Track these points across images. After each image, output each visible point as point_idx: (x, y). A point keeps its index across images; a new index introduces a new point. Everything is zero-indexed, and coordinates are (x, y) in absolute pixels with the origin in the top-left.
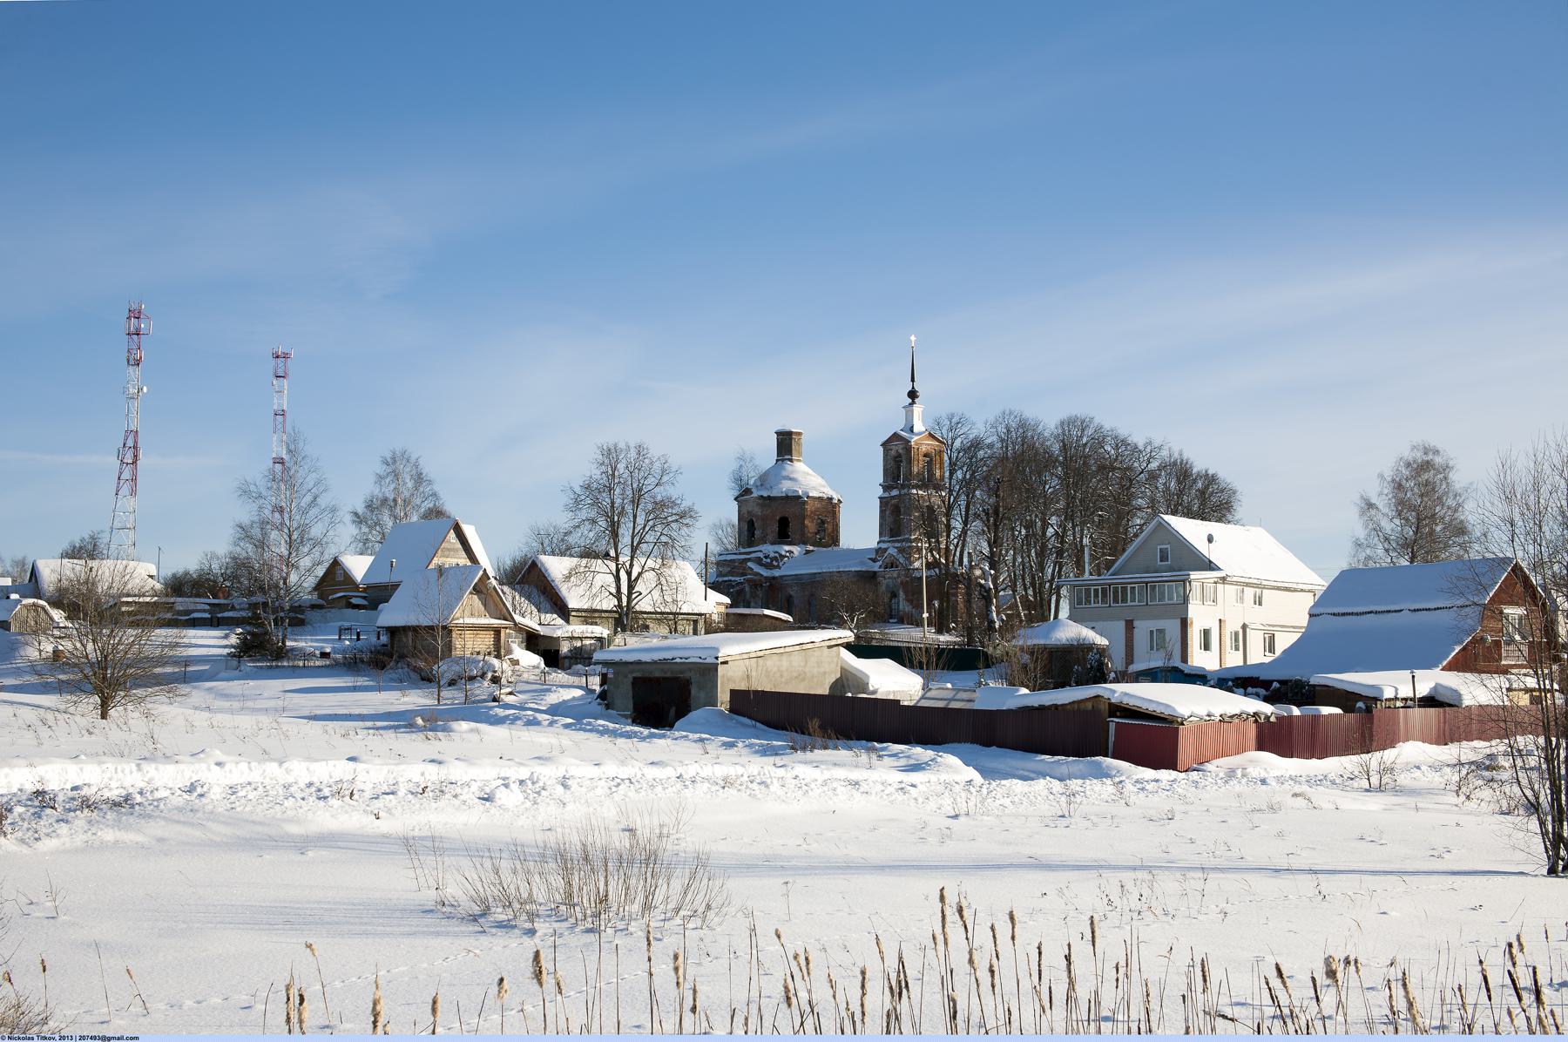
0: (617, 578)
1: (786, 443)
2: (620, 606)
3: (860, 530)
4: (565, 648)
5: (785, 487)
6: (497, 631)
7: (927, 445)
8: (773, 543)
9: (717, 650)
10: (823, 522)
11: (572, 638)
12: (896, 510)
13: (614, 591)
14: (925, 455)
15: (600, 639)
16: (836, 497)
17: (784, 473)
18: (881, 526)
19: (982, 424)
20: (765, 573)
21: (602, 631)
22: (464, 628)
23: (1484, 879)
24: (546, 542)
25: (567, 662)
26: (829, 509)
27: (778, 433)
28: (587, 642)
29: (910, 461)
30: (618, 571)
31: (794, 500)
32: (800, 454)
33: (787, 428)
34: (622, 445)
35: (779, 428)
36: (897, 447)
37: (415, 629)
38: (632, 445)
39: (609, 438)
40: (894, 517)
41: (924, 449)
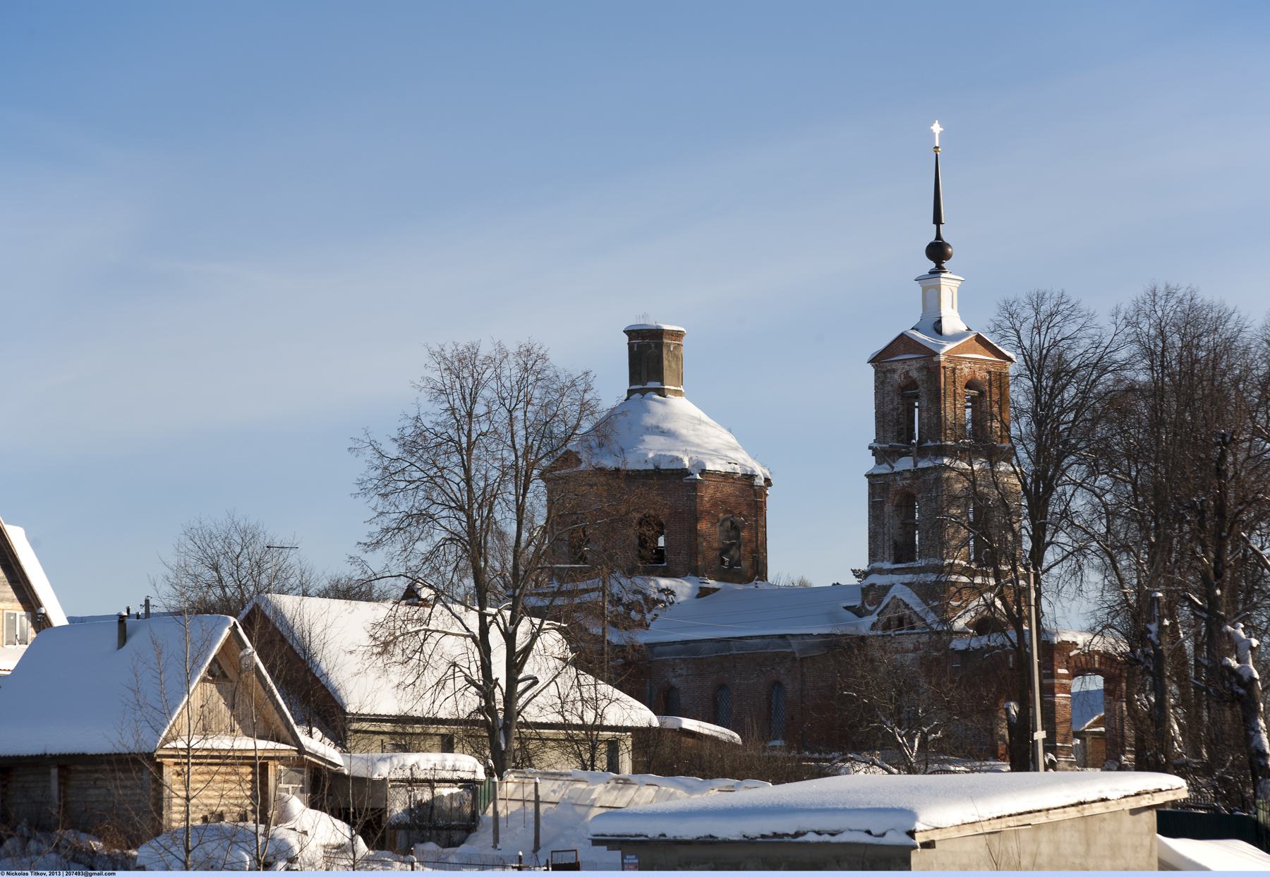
0: (485, 650)
1: (649, 355)
2: (489, 709)
3: (820, 543)
4: (398, 806)
5: (652, 450)
6: (260, 767)
7: (974, 363)
8: (631, 572)
9: (912, 815)
10: (735, 528)
11: (412, 782)
12: (906, 501)
13: (477, 675)
14: (969, 385)
15: (469, 784)
16: (760, 471)
17: (649, 421)
19: (1105, 315)
20: (614, 637)
21: (467, 764)
22: (188, 757)
24: (225, 565)
25: (401, 836)
26: (749, 496)
27: (632, 333)
28: (445, 791)
29: (936, 397)
30: (484, 629)
31: (675, 480)
32: (680, 380)
33: (653, 322)
34: (486, 350)
35: (634, 321)
37: (68, 764)
38: (512, 348)
39: (455, 339)
40: (901, 515)
41: (965, 370)
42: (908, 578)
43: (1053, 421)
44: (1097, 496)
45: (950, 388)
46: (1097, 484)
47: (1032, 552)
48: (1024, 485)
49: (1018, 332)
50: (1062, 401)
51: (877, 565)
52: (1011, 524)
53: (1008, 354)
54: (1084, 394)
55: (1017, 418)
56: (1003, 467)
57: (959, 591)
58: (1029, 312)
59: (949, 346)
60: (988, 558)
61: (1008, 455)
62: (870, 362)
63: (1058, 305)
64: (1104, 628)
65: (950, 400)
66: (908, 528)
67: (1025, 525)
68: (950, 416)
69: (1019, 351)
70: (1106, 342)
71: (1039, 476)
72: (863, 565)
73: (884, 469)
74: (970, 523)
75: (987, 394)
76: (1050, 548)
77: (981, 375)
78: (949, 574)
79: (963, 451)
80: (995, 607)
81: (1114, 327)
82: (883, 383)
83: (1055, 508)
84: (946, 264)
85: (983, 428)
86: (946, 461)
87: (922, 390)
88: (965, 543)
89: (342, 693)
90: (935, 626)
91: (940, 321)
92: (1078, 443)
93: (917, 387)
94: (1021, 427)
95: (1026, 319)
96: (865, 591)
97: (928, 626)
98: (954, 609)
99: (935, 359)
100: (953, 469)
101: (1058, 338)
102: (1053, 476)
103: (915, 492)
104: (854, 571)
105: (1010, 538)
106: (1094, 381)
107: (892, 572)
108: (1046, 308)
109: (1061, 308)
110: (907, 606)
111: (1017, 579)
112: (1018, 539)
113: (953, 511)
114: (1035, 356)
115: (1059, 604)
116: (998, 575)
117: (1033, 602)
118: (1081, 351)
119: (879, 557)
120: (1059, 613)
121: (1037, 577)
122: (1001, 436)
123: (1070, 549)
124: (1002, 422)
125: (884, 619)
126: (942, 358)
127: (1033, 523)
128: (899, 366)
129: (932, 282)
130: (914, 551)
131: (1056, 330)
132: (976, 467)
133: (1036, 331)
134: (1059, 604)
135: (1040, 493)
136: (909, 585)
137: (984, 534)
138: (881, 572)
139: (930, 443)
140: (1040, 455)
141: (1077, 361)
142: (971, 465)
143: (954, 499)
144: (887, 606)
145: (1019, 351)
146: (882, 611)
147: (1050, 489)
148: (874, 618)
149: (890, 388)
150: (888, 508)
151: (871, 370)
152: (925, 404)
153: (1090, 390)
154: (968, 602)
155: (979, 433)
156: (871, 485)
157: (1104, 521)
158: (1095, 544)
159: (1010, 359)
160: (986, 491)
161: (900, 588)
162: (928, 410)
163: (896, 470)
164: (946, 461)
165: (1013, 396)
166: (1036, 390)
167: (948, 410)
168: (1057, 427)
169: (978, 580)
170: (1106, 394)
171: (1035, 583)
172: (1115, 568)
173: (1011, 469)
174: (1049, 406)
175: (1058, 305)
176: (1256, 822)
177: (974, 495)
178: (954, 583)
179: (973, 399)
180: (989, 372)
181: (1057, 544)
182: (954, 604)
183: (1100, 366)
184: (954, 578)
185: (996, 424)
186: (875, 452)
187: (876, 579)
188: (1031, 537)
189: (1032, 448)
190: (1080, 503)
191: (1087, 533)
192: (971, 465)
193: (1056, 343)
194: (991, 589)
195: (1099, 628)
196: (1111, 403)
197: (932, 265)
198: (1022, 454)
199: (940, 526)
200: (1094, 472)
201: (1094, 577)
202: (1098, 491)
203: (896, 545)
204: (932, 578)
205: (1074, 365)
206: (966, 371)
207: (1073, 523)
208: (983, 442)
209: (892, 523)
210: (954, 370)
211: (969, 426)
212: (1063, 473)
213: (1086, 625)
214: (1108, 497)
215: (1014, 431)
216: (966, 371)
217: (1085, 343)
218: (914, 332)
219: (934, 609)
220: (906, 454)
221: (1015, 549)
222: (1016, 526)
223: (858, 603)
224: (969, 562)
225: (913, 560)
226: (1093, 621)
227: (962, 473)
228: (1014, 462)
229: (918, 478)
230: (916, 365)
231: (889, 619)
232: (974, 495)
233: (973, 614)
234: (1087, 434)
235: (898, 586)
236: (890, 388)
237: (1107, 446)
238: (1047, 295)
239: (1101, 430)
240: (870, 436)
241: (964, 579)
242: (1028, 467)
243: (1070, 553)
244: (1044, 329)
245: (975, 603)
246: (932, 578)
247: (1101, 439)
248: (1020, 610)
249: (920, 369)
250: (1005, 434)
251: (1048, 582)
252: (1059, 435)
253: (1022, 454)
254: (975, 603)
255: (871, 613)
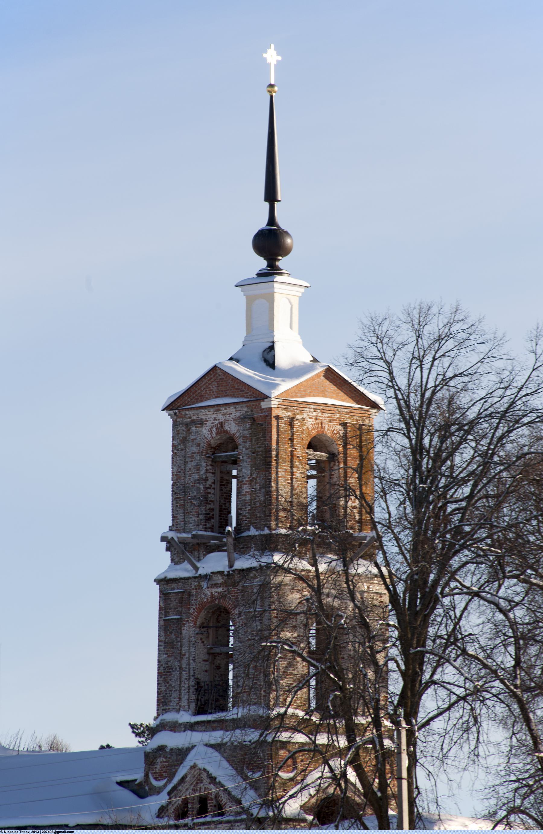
7: (321, 412)
12: (217, 619)
14: (314, 444)
18: (165, 673)
23: (289, 322)
29: (264, 461)
34: (205, 650)
36: (221, 416)
41: (309, 423)
42: (216, 736)
43: (439, 498)
44: (501, 611)
45: (285, 448)
46: (501, 593)
47: (403, 695)
48: (394, 597)
49: (389, 364)
50: (452, 467)
51: (170, 717)
52: (374, 653)
53: (373, 397)
54: (487, 459)
55: (384, 494)
56: (363, 567)
57: (293, 757)
58: (406, 334)
59: (285, 386)
60: (337, 703)
61: (370, 550)
62: (167, 408)
63: (450, 324)
64: (513, 811)
65: (284, 466)
66: (218, 659)
67: (393, 657)
68: (284, 489)
69: (391, 393)
70: (520, 380)
71: (416, 582)
72: (148, 716)
73: (184, 571)
74: (310, 653)
75: (338, 459)
76: (430, 691)
77: (332, 430)
78: (278, 730)
79: (304, 543)
80: (347, 781)
81: (532, 357)
82: (184, 441)
83: (437, 628)
84: (282, 262)
85: (334, 508)
86: (278, 558)
87: (243, 451)
88: (303, 682)
89: (297, 364)
90: (255, 811)
91: (272, 348)
92: (474, 531)
93: (235, 448)
94: (391, 507)
95: (403, 345)
96: (150, 758)
97: (246, 811)
98: (286, 784)
99: (264, 405)
100: (288, 571)
101: (450, 374)
102: (436, 582)
103: (228, 604)
104: (133, 727)
105: (371, 675)
106: (501, 438)
107: (192, 727)
108: (432, 329)
109: (455, 328)
110: (213, 780)
111: (380, 737)
112: (382, 674)
113: (287, 634)
114: (415, 401)
115: (443, 777)
116: (351, 732)
117: (405, 774)
118: (483, 394)
119: (173, 704)
120: (443, 789)
121: (411, 734)
122: (360, 521)
123: (460, 692)
124: (362, 498)
125: (178, 800)
126: (274, 404)
127: (405, 652)
128: (209, 415)
129: (262, 288)
130: (225, 696)
131: (446, 361)
132: (322, 568)
133: (416, 363)
134: (443, 777)
135: (416, 605)
136: (217, 747)
137: (331, 668)
138: (174, 727)
139: (253, 532)
140: (420, 552)
141: (476, 409)
142: (315, 564)
143: (287, 616)
144: (183, 779)
145: (391, 393)
146: (174, 788)
147: (431, 601)
148: (162, 799)
149: (194, 449)
150: (189, 630)
151: (166, 422)
152: (247, 470)
153: (493, 454)
154: (305, 773)
155: (327, 516)
156: (164, 596)
157: (511, 649)
158: (497, 683)
159: (375, 405)
160: (336, 603)
161: (204, 753)
162: (252, 481)
163: (201, 572)
164: (278, 558)
165: (378, 460)
166: (414, 453)
167: (281, 481)
168: (445, 505)
169: (322, 739)
170: (519, 458)
171: (408, 745)
172: (528, 721)
173: (375, 571)
174: (434, 474)
175: (450, 324)
176: (428, 627)
177: (319, 610)
178: (284, 745)
179: (319, 466)
180: (344, 425)
181: (443, 684)
182: (285, 775)
183: (508, 416)
184: (284, 736)
185: (353, 503)
186: (170, 544)
187: (169, 740)
188: (404, 674)
189: (406, 537)
190: (477, 621)
191: (486, 666)
192: (315, 564)
193: (445, 382)
194: (341, 753)
195: (502, 813)
196: (525, 472)
197: (262, 263)
198: (392, 548)
199: (266, 657)
200: (498, 574)
201: (496, 735)
202: (503, 604)
203: (199, 687)
204: (253, 735)
205: (471, 414)
206: (310, 423)
207: (464, 651)
208: (335, 531)
209: (194, 652)
210: (291, 422)
211: (313, 507)
212: (453, 577)
213: (483, 808)
214: (519, 613)
215: (379, 514)
216: (310, 423)
217: (488, 382)
218: (233, 365)
219: (254, 786)
220: (217, 548)
221: (377, 691)
222: (381, 658)
223: (139, 776)
224: (309, 712)
225: (224, 709)
226: (493, 801)
227: (300, 577)
228: (380, 559)
229: (235, 584)
230: (234, 413)
231: (185, 802)
232: (319, 610)
233: (313, 791)
234: (486, 522)
235: (201, 749)
236: (194, 449)
237: (519, 536)
238: (434, 310)
239: (508, 513)
240: (163, 520)
241: (300, 738)
242: (401, 567)
243: (461, 698)
244: (428, 359)
245: (316, 774)
246: (253, 735)
247: (510, 525)
248: (383, 786)
249: (240, 420)
250: (366, 517)
251: (428, 743)
252: (447, 519)
253: (392, 548)
254: (316, 774)
255: (158, 791)
